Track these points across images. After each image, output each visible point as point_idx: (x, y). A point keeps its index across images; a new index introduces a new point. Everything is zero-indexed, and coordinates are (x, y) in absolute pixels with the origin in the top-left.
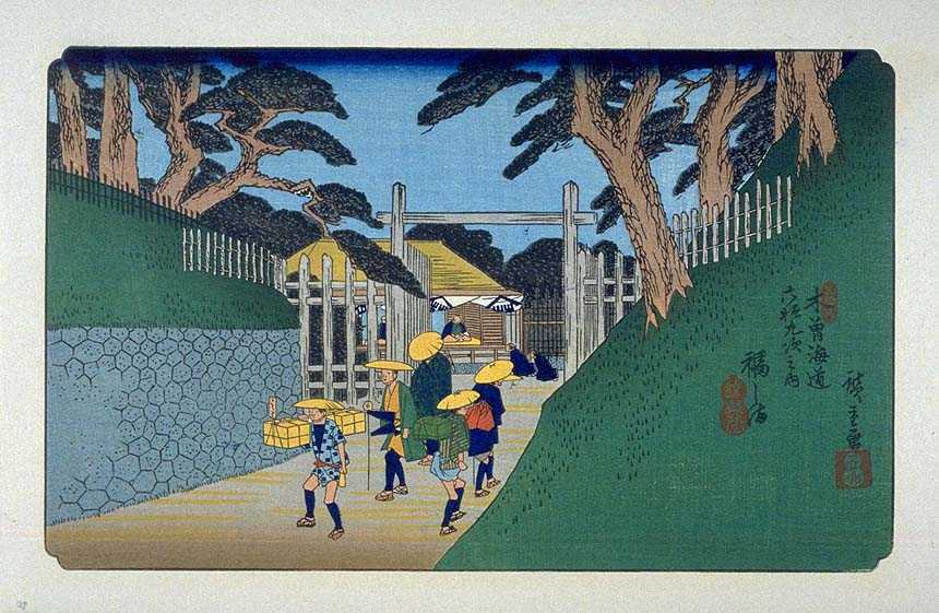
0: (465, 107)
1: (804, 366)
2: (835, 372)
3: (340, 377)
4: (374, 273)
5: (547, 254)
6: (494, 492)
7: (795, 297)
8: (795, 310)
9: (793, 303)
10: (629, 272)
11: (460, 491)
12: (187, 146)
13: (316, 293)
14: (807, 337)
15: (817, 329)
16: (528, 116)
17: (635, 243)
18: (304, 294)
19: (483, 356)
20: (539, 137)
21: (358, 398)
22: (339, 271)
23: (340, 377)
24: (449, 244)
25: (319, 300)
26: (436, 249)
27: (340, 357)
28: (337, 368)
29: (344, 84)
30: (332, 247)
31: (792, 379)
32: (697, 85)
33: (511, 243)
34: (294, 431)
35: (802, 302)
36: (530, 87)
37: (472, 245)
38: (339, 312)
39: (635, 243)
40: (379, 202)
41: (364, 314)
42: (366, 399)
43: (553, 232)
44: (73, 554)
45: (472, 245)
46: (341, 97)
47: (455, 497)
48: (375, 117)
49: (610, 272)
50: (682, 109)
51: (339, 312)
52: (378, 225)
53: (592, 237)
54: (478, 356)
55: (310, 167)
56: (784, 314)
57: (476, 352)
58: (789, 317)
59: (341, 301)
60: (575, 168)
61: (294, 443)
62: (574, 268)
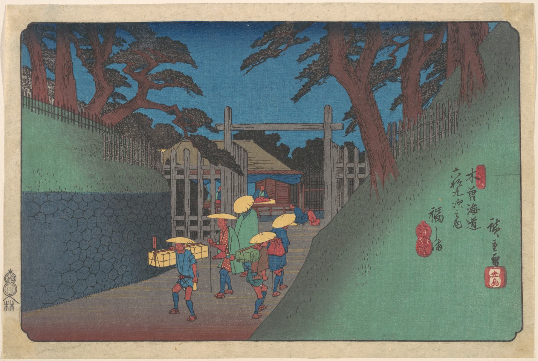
0: (265, 59)
1: (465, 217)
2: (483, 221)
3: (194, 223)
4: (214, 161)
5: (316, 147)
6: (284, 292)
7: (460, 174)
8: (459, 182)
9: (458, 178)
10: (362, 160)
11: (264, 294)
12: (105, 84)
13: (181, 172)
14: (466, 198)
15: (472, 193)
16: (304, 65)
17: (366, 141)
18: (174, 173)
19: (277, 210)
20: (312, 78)
21: (204, 237)
22: (194, 161)
23: (194, 223)
24: (256, 142)
25: (183, 176)
26: (250, 146)
27: (194, 211)
28: (179, 218)
29: (195, 48)
30: (188, 144)
31: (457, 224)
32: (403, 45)
33: (295, 141)
34: (167, 257)
35: (463, 178)
36: (308, 45)
37: (268, 142)
38: (194, 184)
39: (366, 141)
40: (217, 120)
41: (209, 185)
42: (209, 236)
43: (320, 135)
44: (38, 331)
45: (268, 142)
46: (194, 56)
47: (261, 296)
48: (210, 67)
49: (351, 160)
50: (393, 60)
51: (194, 184)
52: (216, 131)
53: (340, 139)
54: (275, 210)
55: (179, 97)
56: (453, 184)
57: (273, 208)
58: (456, 185)
59: (195, 177)
60: (333, 96)
61: (166, 264)
62: (331, 157)
